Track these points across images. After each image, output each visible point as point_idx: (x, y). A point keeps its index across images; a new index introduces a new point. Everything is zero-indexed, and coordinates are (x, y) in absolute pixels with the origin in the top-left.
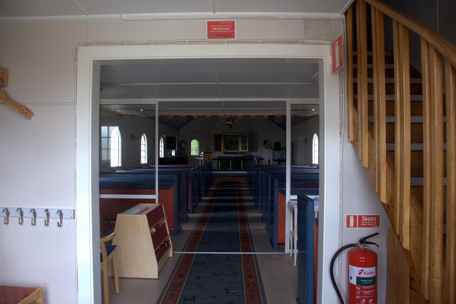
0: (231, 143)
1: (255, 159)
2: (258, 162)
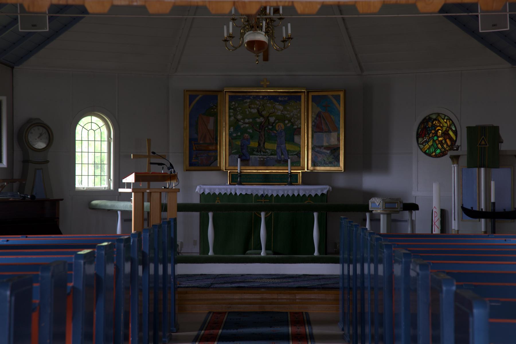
0: (265, 131)
1: (376, 205)
2: (391, 222)
